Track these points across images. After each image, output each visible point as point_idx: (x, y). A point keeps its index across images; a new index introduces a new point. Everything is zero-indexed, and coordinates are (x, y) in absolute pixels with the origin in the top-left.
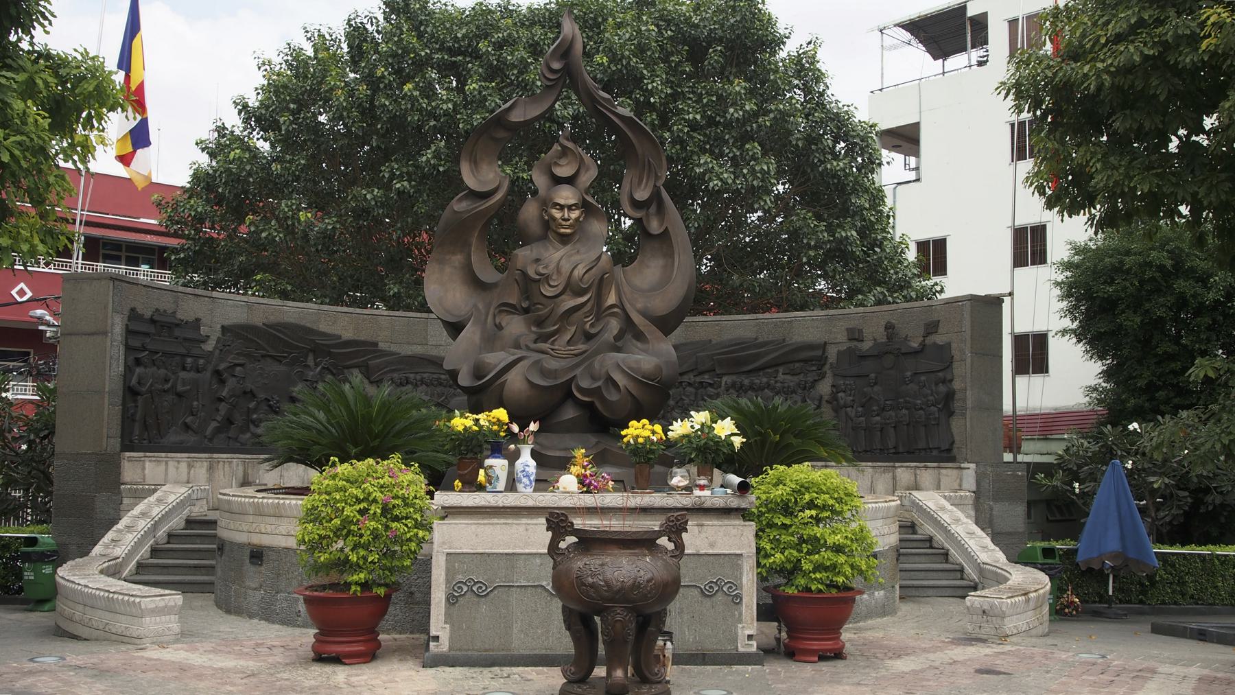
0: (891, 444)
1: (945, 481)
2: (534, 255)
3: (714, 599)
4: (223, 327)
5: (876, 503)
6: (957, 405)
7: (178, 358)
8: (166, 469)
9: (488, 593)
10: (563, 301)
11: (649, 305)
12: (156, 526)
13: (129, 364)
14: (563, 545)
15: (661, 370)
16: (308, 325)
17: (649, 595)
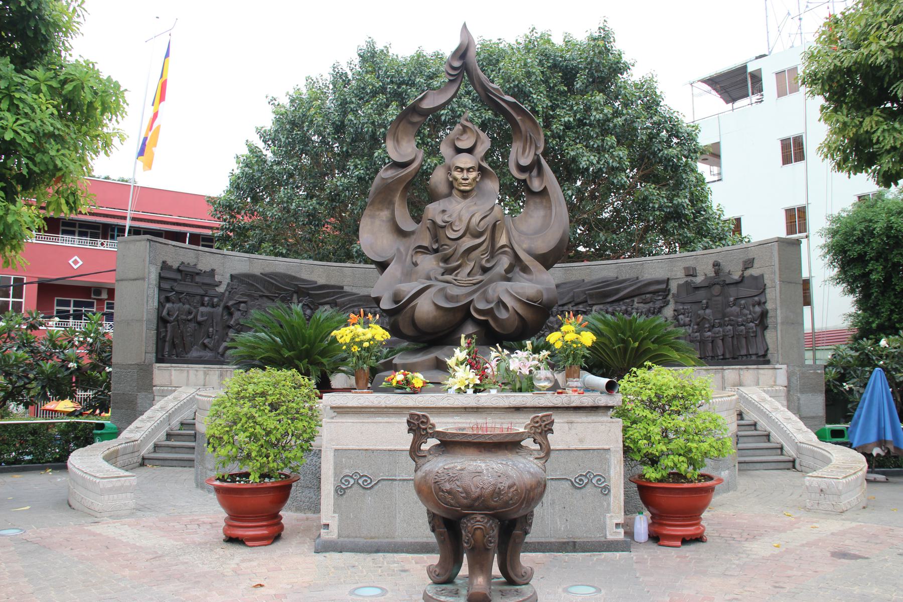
0: (720, 352)
1: (762, 379)
2: (442, 208)
3: (583, 491)
4: (232, 276)
5: (722, 397)
6: (770, 321)
7: (198, 297)
8: (188, 376)
9: (372, 487)
10: (464, 242)
11: (533, 245)
12: (170, 417)
13: (162, 301)
14: (424, 447)
15: (542, 295)
16: (293, 274)
17: (511, 502)
